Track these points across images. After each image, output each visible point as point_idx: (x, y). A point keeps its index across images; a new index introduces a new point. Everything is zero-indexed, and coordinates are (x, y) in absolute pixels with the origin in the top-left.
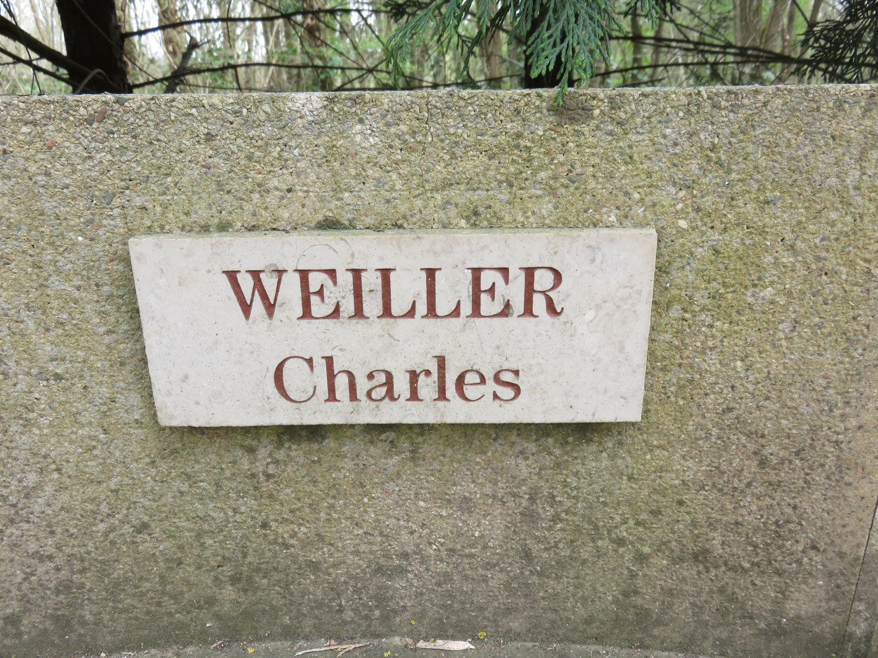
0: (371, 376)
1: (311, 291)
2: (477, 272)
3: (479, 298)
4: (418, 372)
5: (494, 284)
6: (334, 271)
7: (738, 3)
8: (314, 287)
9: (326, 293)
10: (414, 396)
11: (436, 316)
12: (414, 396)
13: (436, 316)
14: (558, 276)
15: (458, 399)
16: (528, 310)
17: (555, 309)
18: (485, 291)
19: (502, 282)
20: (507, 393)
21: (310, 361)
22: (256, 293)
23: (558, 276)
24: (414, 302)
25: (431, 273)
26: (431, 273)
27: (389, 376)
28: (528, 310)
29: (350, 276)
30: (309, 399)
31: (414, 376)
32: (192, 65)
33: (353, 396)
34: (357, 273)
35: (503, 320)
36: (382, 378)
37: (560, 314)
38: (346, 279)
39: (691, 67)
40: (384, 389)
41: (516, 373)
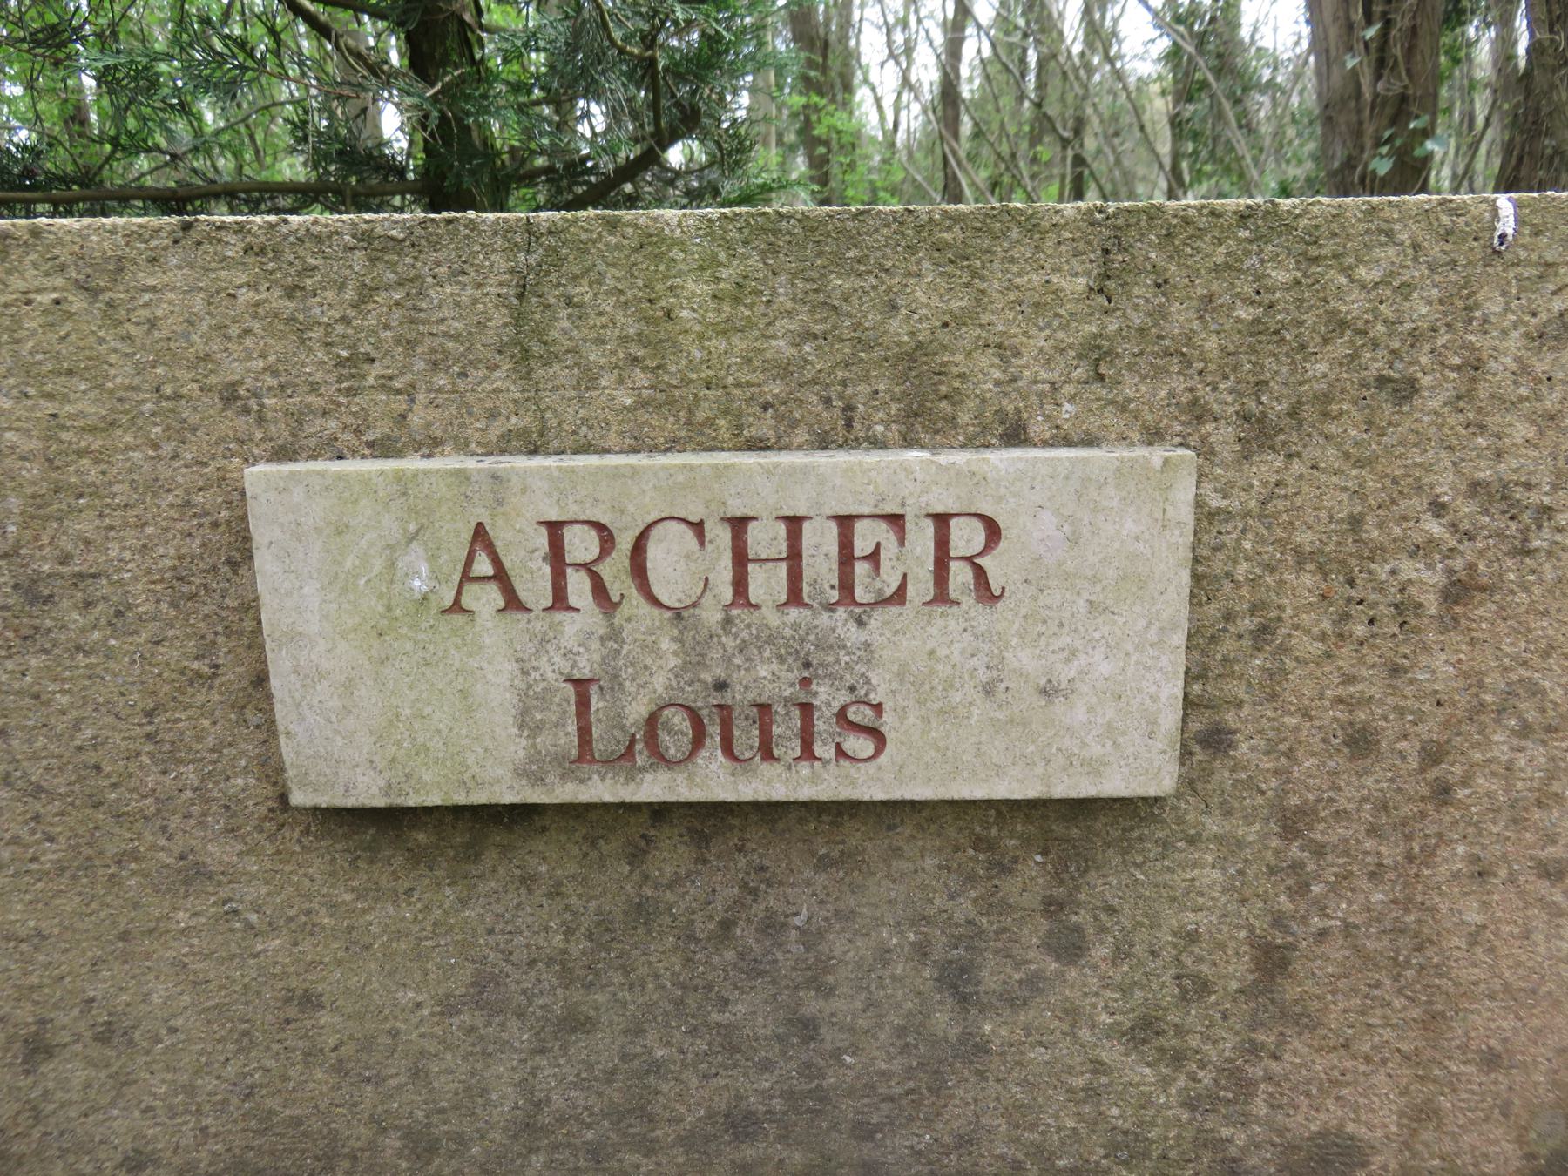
5: (878, 544)
6: (900, 517)
7: (985, 5)
8: (862, 546)
9: (885, 565)
14: (993, 531)
16: (941, 596)
17: (988, 588)
20: (860, 745)
21: (698, 527)
23: (993, 531)
28: (941, 596)
29: (929, 528)
33: (808, 753)
34: (794, 523)
35: (894, 610)
37: (620, 603)
38: (922, 538)
39: (268, 102)
41: (878, 708)
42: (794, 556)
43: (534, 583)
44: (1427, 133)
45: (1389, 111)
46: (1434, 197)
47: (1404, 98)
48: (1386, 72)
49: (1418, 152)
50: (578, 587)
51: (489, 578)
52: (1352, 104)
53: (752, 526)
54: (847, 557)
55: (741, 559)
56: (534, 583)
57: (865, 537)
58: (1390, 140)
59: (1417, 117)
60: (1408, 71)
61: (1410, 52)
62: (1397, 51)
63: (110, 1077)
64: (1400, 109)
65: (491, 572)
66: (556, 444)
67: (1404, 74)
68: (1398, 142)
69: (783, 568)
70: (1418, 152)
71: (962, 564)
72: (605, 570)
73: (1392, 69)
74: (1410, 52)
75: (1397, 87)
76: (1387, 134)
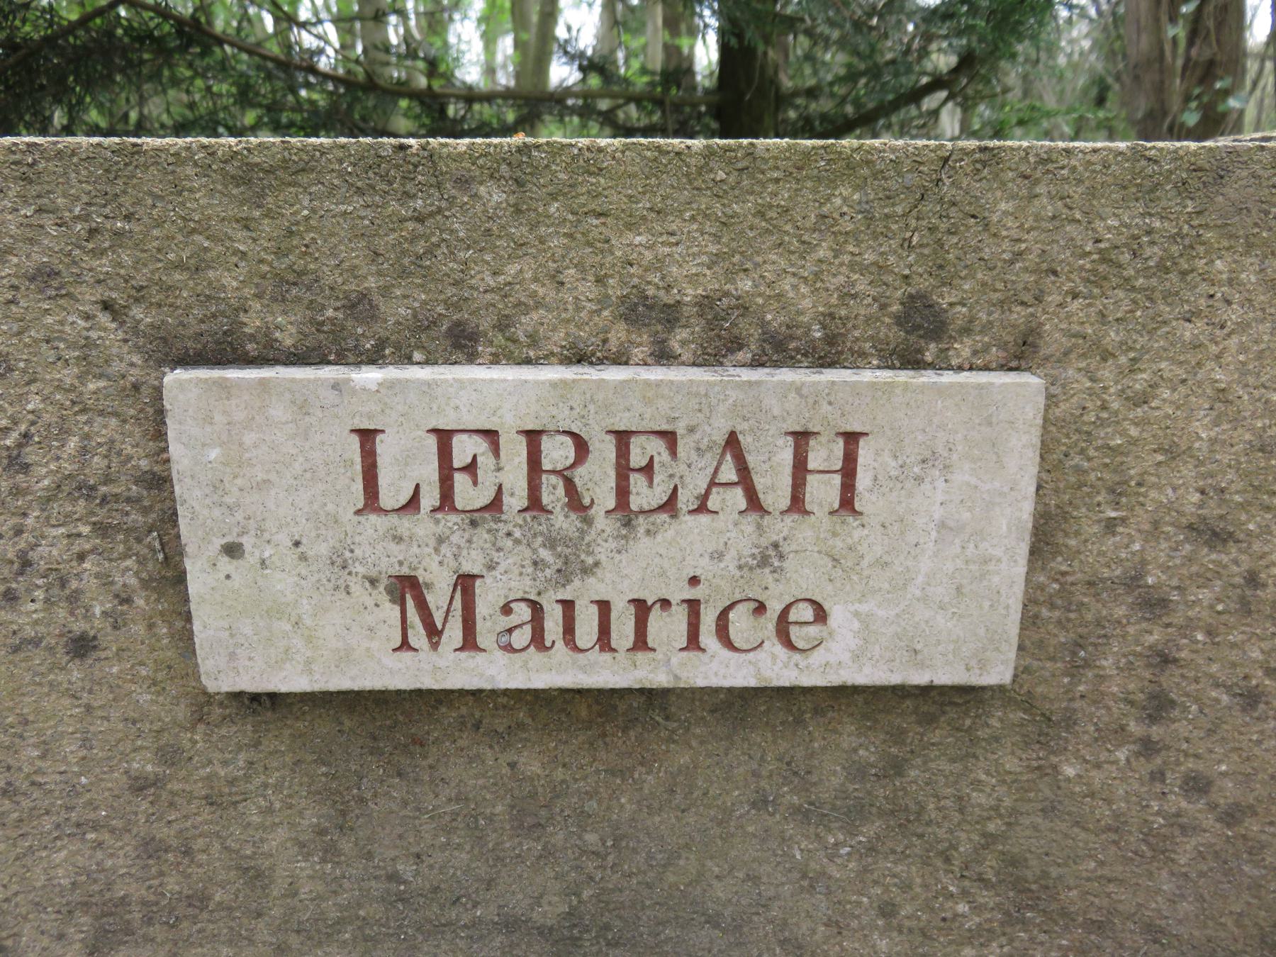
0: (507, 610)
1: (632, 465)
2: (444, 437)
3: (628, 478)
4: (649, 603)
8: (459, 459)
10: (641, 643)
11: (454, 509)
12: (641, 643)
13: (454, 509)
15: (726, 653)
18: (640, 470)
19: (666, 456)
22: (728, 457)
24: (417, 486)
25: (367, 436)
26: (367, 436)
27: (536, 608)
29: (522, 442)
30: (755, 649)
31: (641, 608)
32: (947, 64)
36: (523, 612)
38: (515, 452)
40: (528, 630)
42: (800, 468)
43: (775, 484)
44: (1226, 93)
45: (1199, 72)
46: (932, 142)
47: (1211, 64)
48: (1198, 42)
49: (1221, 108)
50: (552, 493)
51: (736, 484)
52: (1157, 65)
53: (379, 438)
54: (623, 470)
55: (849, 471)
56: (775, 484)
57: (464, 449)
58: (1198, 97)
59: (1222, 78)
60: (1218, 41)
61: (1220, 25)
62: (1211, 24)
63: (766, 935)
64: (1208, 72)
65: (735, 478)
66: (954, 362)
67: (1214, 43)
68: (1205, 99)
69: (837, 480)
70: (1221, 108)
71: (554, 479)
72: (581, 475)
73: (1205, 38)
74: (1220, 25)
75: (1207, 54)
76: (1197, 91)
